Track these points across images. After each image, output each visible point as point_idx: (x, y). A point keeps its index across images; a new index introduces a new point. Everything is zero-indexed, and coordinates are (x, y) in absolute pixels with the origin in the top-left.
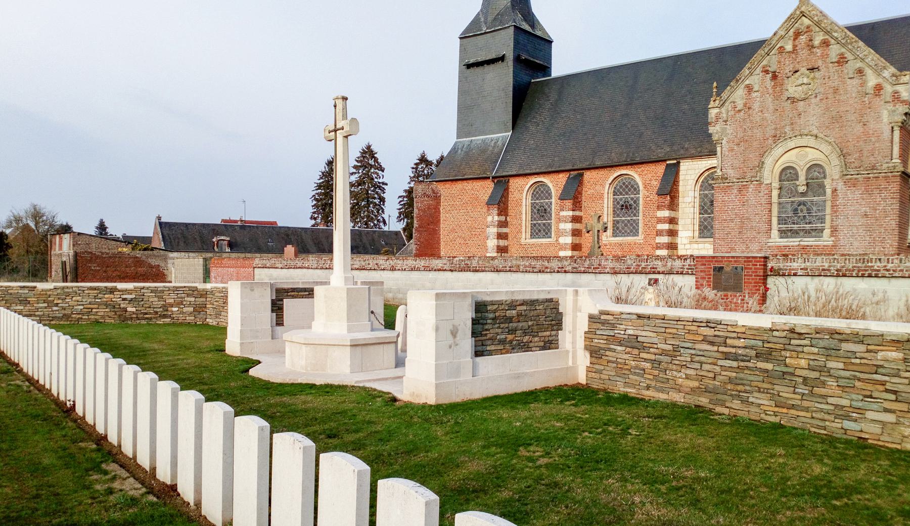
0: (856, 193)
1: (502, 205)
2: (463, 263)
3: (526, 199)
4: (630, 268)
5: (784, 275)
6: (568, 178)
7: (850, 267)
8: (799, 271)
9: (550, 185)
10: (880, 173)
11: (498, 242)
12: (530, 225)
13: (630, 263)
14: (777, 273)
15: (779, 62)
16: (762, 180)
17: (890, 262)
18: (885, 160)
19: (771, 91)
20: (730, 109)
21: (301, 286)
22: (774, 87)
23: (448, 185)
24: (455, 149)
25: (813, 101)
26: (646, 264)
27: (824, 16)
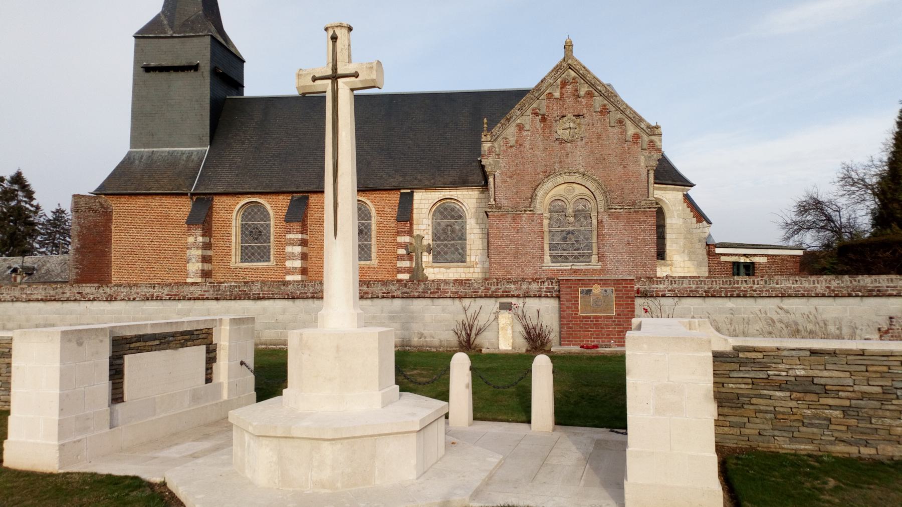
1: (206, 225)
2: (237, 290)
3: (236, 219)
4: (478, 292)
5: (652, 296)
6: (291, 200)
7: (718, 288)
8: (667, 292)
9: (268, 207)
10: (640, 208)
11: (203, 266)
12: (240, 248)
13: (477, 287)
14: (645, 295)
15: (548, 107)
16: (535, 210)
17: (756, 283)
18: (643, 197)
19: (541, 132)
20: (502, 144)
21: (149, 331)
22: (544, 128)
23: (123, 200)
24: (129, 158)
25: (579, 143)
26: (496, 287)
27: (587, 70)
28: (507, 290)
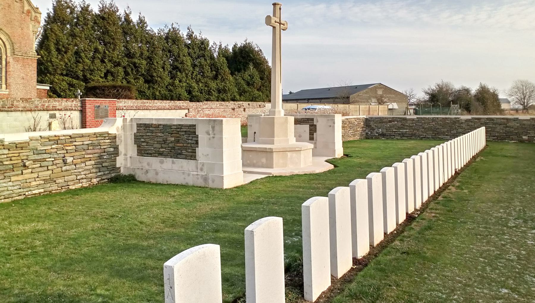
0: (19, 66)
26: (48, 104)
28: (54, 106)
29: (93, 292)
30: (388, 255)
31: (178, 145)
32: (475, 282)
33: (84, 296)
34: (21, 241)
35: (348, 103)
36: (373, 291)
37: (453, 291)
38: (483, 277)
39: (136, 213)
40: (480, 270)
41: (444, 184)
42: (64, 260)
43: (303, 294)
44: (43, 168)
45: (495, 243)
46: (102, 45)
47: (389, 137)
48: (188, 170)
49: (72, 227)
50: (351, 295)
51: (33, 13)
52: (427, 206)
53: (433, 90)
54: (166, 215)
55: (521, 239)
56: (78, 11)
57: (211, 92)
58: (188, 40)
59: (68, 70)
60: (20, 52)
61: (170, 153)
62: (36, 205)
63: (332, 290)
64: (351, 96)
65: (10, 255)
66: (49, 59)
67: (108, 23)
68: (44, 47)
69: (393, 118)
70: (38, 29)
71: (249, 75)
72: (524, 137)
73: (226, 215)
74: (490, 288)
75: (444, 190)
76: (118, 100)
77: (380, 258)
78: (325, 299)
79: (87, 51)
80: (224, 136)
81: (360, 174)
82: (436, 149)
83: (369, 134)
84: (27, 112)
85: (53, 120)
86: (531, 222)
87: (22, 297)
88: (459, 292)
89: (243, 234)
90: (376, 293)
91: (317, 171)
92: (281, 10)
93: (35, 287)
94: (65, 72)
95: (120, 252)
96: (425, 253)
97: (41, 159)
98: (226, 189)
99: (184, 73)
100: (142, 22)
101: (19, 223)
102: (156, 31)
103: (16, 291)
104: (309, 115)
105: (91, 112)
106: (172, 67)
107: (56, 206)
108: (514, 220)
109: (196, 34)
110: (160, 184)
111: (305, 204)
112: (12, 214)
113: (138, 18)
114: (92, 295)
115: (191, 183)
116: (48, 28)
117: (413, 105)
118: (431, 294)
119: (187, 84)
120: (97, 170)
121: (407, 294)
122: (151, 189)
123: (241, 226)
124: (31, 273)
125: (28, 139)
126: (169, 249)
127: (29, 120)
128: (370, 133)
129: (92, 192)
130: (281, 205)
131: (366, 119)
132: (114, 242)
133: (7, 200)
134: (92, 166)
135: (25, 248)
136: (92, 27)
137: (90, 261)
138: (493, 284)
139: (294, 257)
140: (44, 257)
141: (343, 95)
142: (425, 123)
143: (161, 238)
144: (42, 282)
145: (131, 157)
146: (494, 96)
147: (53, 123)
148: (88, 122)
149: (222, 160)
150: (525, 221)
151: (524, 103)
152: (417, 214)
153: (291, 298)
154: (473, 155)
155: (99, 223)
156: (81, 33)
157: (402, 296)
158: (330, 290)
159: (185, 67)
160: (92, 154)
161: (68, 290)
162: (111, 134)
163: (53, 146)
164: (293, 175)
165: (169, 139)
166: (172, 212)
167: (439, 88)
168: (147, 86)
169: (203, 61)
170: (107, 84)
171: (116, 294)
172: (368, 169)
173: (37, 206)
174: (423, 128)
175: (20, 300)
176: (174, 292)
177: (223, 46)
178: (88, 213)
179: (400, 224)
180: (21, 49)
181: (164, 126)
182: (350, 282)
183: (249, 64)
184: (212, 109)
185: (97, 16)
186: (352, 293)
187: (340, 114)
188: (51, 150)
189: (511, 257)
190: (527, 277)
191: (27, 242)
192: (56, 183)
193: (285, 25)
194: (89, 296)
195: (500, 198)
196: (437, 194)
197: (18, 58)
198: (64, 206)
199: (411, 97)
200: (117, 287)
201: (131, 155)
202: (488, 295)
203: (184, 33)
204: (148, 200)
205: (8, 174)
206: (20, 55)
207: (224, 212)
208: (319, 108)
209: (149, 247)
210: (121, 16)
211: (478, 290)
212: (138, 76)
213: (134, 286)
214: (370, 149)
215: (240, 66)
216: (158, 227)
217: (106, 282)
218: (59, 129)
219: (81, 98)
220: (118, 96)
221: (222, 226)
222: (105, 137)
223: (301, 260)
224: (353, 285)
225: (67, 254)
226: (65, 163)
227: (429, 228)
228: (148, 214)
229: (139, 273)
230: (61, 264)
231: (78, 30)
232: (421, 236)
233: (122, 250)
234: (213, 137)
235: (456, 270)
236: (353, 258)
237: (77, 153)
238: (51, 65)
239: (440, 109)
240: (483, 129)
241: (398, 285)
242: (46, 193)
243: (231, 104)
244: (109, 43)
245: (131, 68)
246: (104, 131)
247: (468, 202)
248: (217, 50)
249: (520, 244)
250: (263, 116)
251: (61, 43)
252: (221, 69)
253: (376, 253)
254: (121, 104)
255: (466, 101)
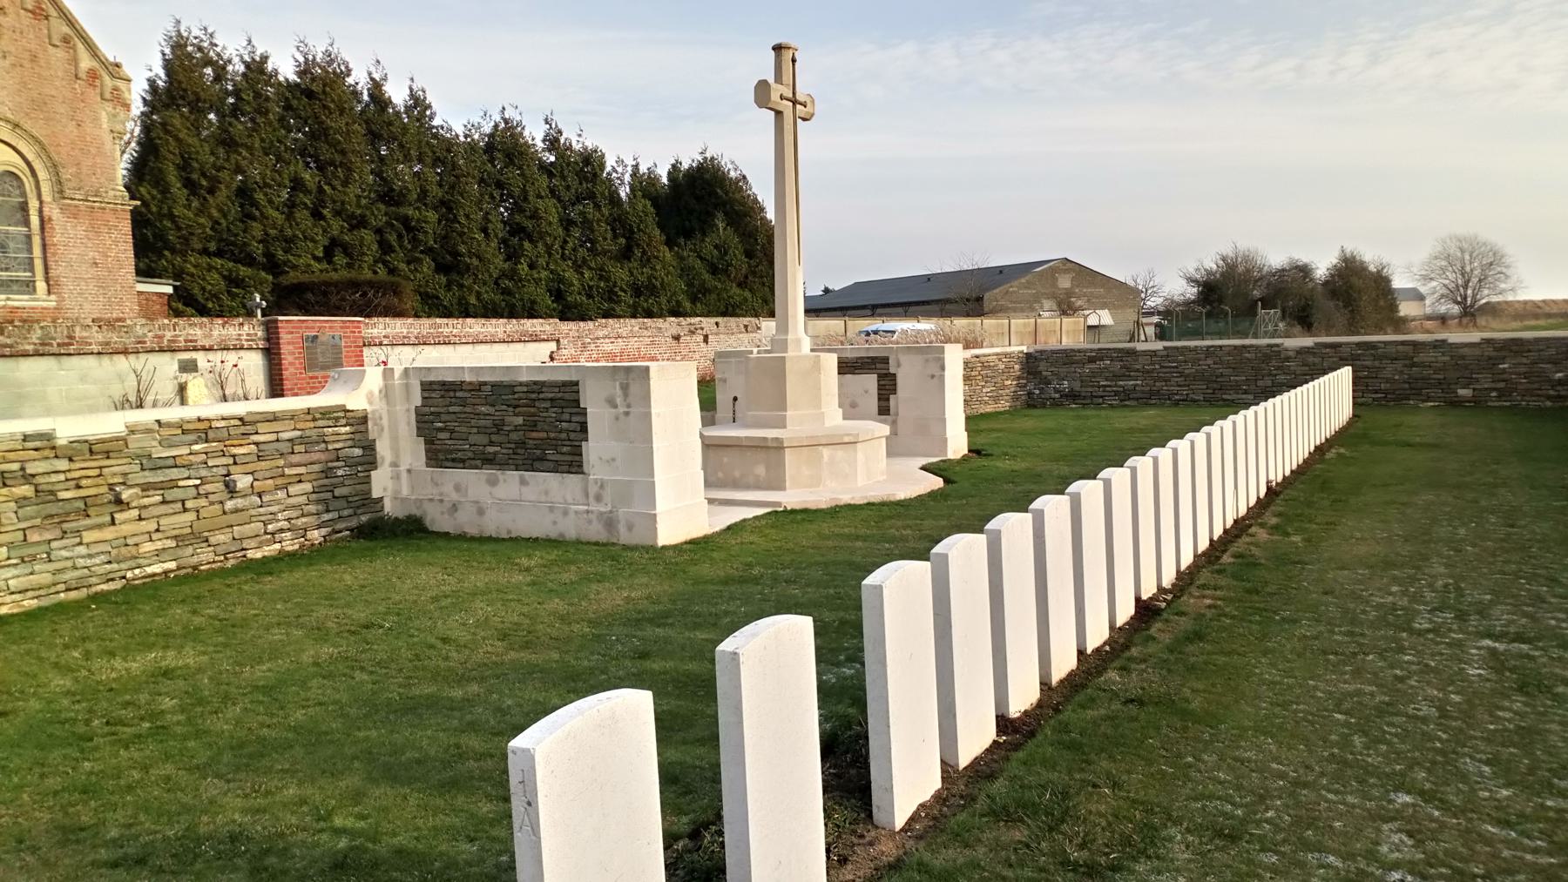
0: (79, 228)
26: (173, 333)
28: (190, 338)
29: (322, 824)
30: (1089, 708)
31: (534, 435)
32: (1322, 774)
33: (301, 836)
34: (119, 700)
35: (980, 313)
36: (1050, 800)
37: (1262, 798)
38: (1345, 763)
39: (429, 615)
40: (1336, 744)
41: (1236, 521)
42: (241, 745)
43: (871, 812)
44: (172, 505)
45: (1375, 674)
46: (311, 168)
47: (1089, 401)
48: (562, 501)
49: (260, 657)
50: (994, 812)
51: (107, 78)
52: (1192, 579)
53: (1209, 273)
54: (511, 619)
55: (1448, 663)
56: (236, 73)
57: (616, 294)
58: (547, 154)
59: (221, 240)
60: (79, 189)
61: (513, 456)
62: (157, 604)
63: (945, 800)
64: (987, 296)
65: (91, 739)
66: (165, 211)
67: (325, 107)
68: (148, 177)
69: (1100, 349)
70: (127, 124)
71: (716, 247)
72: (1461, 392)
73: (667, 615)
74: (1363, 790)
75: (1238, 536)
76: (367, 321)
77: (1068, 714)
78: (926, 822)
79: (270, 187)
80: (656, 409)
81: (1013, 500)
82: (1214, 430)
83: (1035, 396)
84: (116, 357)
85: (191, 378)
86: (1477, 617)
87: (129, 846)
88: (1279, 803)
89: (713, 661)
90: (1058, 804)
91: (901, 495)
92: (797, 64)
93: (165, 819)
94: (213, 246)
95: (392, 717)
96: (1187, 701)
97: (162, 482)
98: (664, 547)
99: (540, 245)
100: (418, 104)
101: (112, 654)
102: (459, 129)
103: (114, 833)
104: (875, 347)
105: (294, 353)
106: (508, 228)
107: (212, 605)
108: (1430, 612)
109: (570, 135)
110: (490, 539)
111: (868, 581)
112: (91, 631)
113: (408, 92)
114: (321, 831)
115: (571, 534)
116: (155, 121)
117: (1152, 314)
118: (1204, 807)
119: (551, 273)
120: (320, 507)
121: (1141, 808)
122: (466, 553)
123: (707, 640)
124: (152, 783)
125: (123, 429)
126: (521, 706)
127: (121, 378)
128: (1037, 392)
129: (311, 565)
130: (808, 585)
131: (1028, 355)
132: (374, 693)
133: (73, 595)
134: (305, 497)
135: (133, 718)
136: (279, 120)
137: (313, 745)
138: (1372, 781)
139: (845, 716)
140: (185, 738)
141: (967, 294)
142: (1185, 362)
143: (498, 678)
144: (184, 806)
145: (409, 471)
146: (1380, 282)
147: (190, 386)
148: (287, 380)
149: (650, 472)
150: (1462, 617)
151: (1465, 298)
152: (1165, 600)
153: (840, 821)
154: (1318, 443)
155: (334, 646)
156: (250, 136)
157: (1128, 811)
158: (938, 798)
159: (544, 227)
160: (302, 466)
161: (255, 821)
162: (352, 411)
163: (196, 447)
164: (837, 506)
165: (508, 419)
166: (525, 609)
167: (1227, 264)
168: (444, 280)
169: (590, 209)
170: (335, 276)
171: (386, 826)
172: (1033, 487)
173: (159, 607)
174: (1181, 374)
175: (125, 854)
176: (538, 814)
177: (643, 169)
178: (301, 620)
179: (1119, 628)
180: (81, 181)
181: (495, 385)
182: (991, 777)
183: (713, 216)
184: (620, 340)
185: (290, 86)
186: (996, 805)
187: (959, 342)
188: (191, 457)
189: (1421, 710)
190: (1465, 763)
191: (137, 702)
192: (209, 546)
193: (808, 105)
194: (314, 835)
195: (1392, 555)
196: (1217, 547)
197: (76, 206)
198: (235, 605)
199: (1149, 292)
200: (387, 808)
201: (411, 464)
202: (1358, 810)
203: (535, 134)
204: (460, 581)
205: (73, 525)
206: (79, 200)
207: (661, 607)
208: (902, 330)
209: (468, 701)
210: (359, 88)
211: (1331, 796)
212: (417, 255)
213: (432, 802)
214: (1040, 433)
215: (690, 221)
216: (489, 648)
217: (357, 797)
218: (209, 402)
219: (263, 316)
220: (367, 310)
221: (656, 642)
222: (337, 419)
223: (864, 723)
224: (999, 786)
225: (250, 729)
226: (231, 489)
227: (1197, 636)
228: (462, 618)
229: (444, 769)
230: (235, 756)
231: (241, 127)
232: (1176, 659)
233: (396, 711)
234: (627, 414)
235: (1270, 744)
236: (997, 717)
237: (263, 463)
238: (174, 227)
239: (1227, 323)
240: (1345, 374)
241: (1115, 783)
242: (183, 572)
243: (670, 325)
244: (332, 163)
245: (396, 231)
246: (333, 404)
247: (1303, 569)
248: (627, 178)
249: (1445, 676)
250: (755, 355)
251: (195, 165)
252: (639, 230)
253: (1058, 703)
254: (375, 331)
255: (1300, 300)
